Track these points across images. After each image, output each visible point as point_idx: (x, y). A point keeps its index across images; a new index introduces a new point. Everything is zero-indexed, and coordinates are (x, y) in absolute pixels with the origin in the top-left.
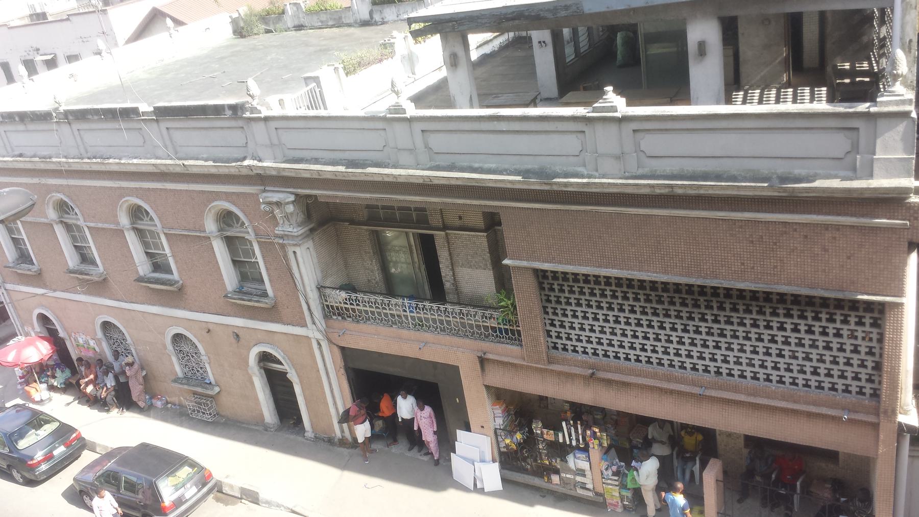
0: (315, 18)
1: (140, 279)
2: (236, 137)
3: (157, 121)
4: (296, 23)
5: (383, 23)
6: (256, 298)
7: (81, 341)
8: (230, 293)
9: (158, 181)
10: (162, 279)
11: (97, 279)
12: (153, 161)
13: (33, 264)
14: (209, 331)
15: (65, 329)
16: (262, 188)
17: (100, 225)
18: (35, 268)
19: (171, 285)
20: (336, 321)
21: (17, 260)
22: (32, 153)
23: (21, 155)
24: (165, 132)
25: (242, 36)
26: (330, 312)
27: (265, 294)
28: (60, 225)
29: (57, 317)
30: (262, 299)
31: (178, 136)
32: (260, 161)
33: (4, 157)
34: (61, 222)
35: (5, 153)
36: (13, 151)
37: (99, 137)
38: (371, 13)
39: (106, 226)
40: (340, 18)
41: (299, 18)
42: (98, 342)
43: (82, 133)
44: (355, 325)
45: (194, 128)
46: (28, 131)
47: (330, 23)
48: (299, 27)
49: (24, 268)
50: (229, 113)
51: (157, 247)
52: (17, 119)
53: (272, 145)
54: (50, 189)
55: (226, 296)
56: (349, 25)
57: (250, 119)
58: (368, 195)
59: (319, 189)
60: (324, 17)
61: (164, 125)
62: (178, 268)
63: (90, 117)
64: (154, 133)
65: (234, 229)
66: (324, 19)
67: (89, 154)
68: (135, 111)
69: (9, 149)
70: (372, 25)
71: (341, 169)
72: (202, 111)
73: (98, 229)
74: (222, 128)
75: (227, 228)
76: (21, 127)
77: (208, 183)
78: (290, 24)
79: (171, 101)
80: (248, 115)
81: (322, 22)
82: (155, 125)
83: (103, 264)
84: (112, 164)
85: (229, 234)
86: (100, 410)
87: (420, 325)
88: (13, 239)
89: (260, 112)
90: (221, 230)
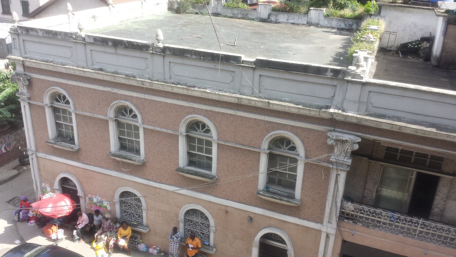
0: (230, 11)
1: (180, 170)
2: (326, 92)
3: (254, 69)
4: (215, 11)
5: (276, 22)
6: (286, 199)
7: (95, 200)
8: (261, 191)
9: (231, 108)
10: (200, 172)
11: (136, 163)
12: (238, 96)
13: (74, 144)
14: (227, 212)
15: (83, 190)
16: (333, 129)
17: (158, 129)
18: (76, 147)
19: (211, 179)
20: (348, 224)
21: (56, 138)
22: (113, 70)
23: (101, 70)
24: (167, 64)
25: (178, 11)
26: (344, 216)
27: (292, 197)
28: (50, 109)
29: (80, 182)
30: (290, 200)
31: (267, 83)
32: (343, 111)
33: (83, 68)
34: (116, 120)
35: (84, 65)
36: (26, 53)
37: (184, 71)
38: (269, 15)
39: (165, 130)
40: (247, 14)
41: (217, 9)
42: (113, 204)
43: (172, 64)
44: (365, 229)
45: (269, 77)
46: (116, 54)
47: (239, 16)
48: (216, 14)
49: (66, 146)
50: (329, 74)
51: (65, 119)
52: (110, 44)
53: (360, 102)
54: (117, 97)
55: (258, 193)
56: (253, 19)
57: (348, 81)
58: (444, 151)
59: (387, 137)
60: (235, 12)
61: (258, 73)
62: (218, 168)
63: (189, 55)
64: (247, 78)
65: (282, 150)
66: (236, 13)
67: (172, 81)
68: (237, 59)
69: (90, 63)
70: (269, 22)
71: (434, 130)
72: (214, 58)
73: (153, 131)
74: (314, 83)
75: (275, 148)
76: (112, 50)
77: (274, 116)
78: (210, 12)
79: (197, 48)
80: (349, 78)
81: (233, 14)
82: (251, 71)
83: (146, 154)
84: (196, 92)
85: (275, 152)
86: (86, 242)
87: (408, 233)
88: (57, 124)
89: (362, 78)
90: (269, 148)
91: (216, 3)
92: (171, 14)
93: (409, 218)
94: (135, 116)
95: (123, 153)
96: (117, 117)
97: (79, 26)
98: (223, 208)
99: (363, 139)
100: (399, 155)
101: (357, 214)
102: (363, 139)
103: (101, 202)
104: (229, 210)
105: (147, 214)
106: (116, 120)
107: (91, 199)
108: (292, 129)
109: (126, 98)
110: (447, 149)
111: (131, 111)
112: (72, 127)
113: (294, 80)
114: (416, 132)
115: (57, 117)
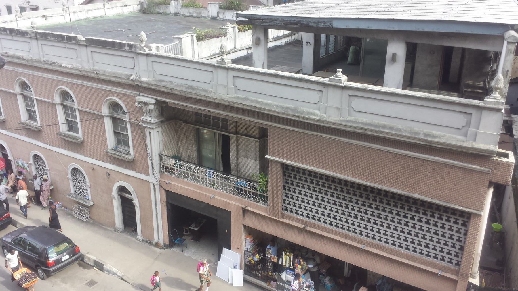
3: (86, 46)
14: (93, 169)
17: (43, 99)
25: (144, 13)
26: (164, 169)
52: (8, 32)
68: (75, 38)
80: (137, 51)
81: (190, 13)
82: (85, 48)
91: (176, 3)
92: (141, 14)
93: (223, 175)
94: (73, 101)
95: (70, 133)
96: (63, 101)
97: (32, 24)
98: (91, 165)
99: (157, 100)
100: (203, 118)
101: (250, 190)
102: (157, 100)
103: (23, 165)
104: (95, 167)
105: (50, 173)
106: (62, 105)
107: (17, 162)
108: (118, 94)
109: (24, 75)
110: (205, 107)
111: (71, 97)
112: (35, 111)
113: (376, 99)
114: (468, 150)
115: (67, 115)
